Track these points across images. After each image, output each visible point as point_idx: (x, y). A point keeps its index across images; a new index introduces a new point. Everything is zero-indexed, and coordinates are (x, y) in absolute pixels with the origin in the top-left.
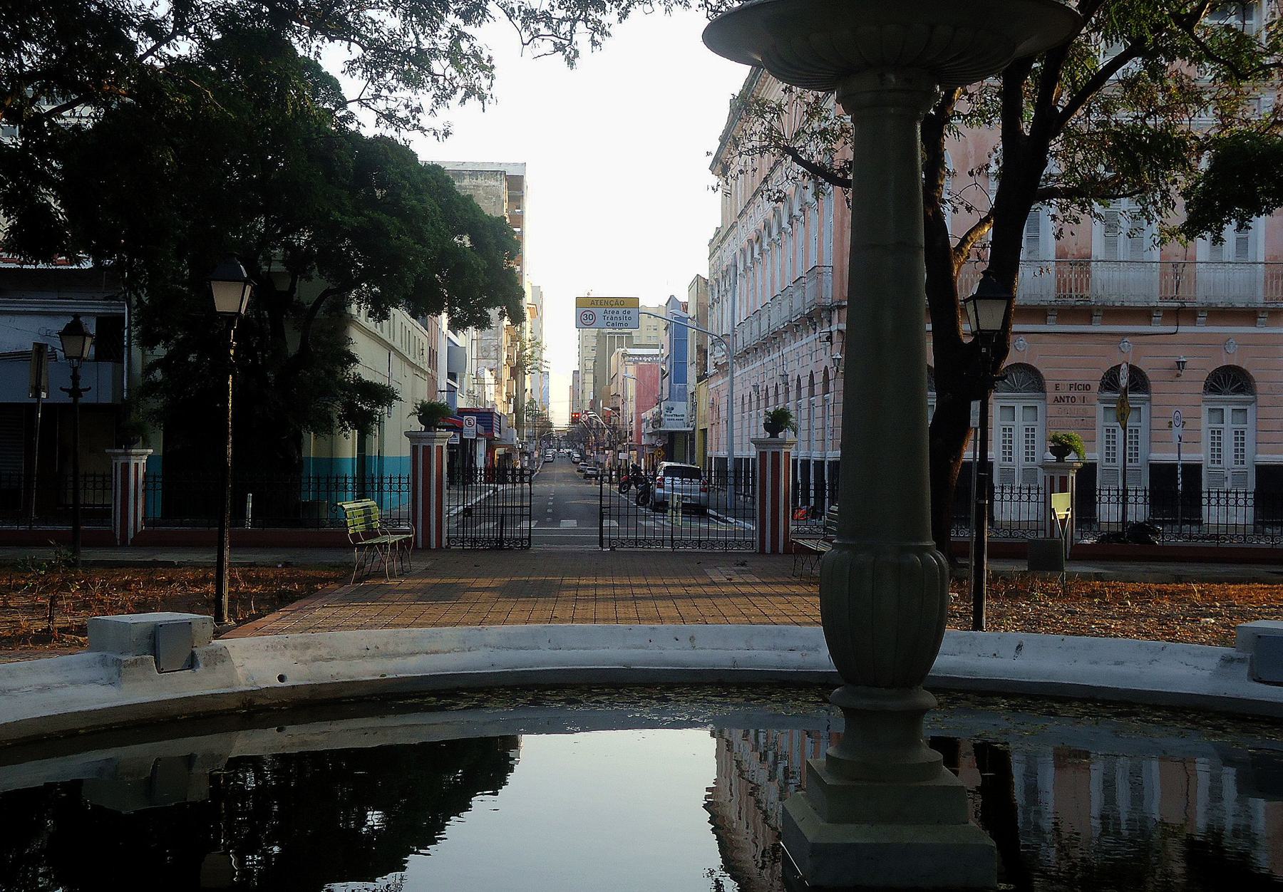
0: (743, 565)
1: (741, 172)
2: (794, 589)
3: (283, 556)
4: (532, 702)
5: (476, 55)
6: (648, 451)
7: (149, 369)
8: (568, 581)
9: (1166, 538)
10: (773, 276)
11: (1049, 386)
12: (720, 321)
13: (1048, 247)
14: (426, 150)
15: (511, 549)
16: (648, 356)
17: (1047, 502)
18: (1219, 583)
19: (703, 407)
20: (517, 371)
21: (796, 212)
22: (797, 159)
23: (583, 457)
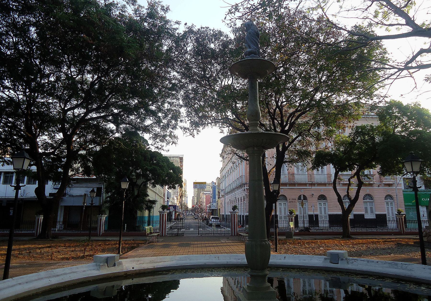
0: (228, 238)
1: (226, 158)
2: (239, 244)
3: (132, 238)
4: (185, 272)
5: (174, 136)
6: (208, 213)
7: (107, 198)
8: (192, 243)
9: (313, 230)
10: (233, 178)
11: (288, 199)
12: (223, 186)
13: (286, 172)
14: (164, 153)
15: (180, 236)
16: (208, 193)
17: (289, 224)
18: (323, 240)
19: (219, 204)
20: (181, 197)
21: (237, 165)
22: (237, 155)
23: (195, 215)
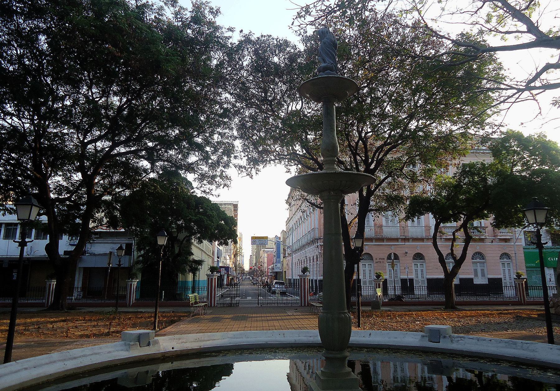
0: (296, 310)
1: (294, 205)
2: (310, 316)
3: (171, 309)
4: (240, 354)
5: (227, 176)
6: (270, 277)
7: (139, 257)
8: (249, 315)
9: (406, 299)
10: (302, 231)
11: (374, 259)
12: (289, 242)
13: (372, 223)
14: (213, 199)
15: (234, 306)
16: (270, 251)
17: (375, 291)
18: (420, 311)
19: (285, 265)
20: (235, 255)
21: (308, 214)
22: (308, 202)
23: (253, 279)
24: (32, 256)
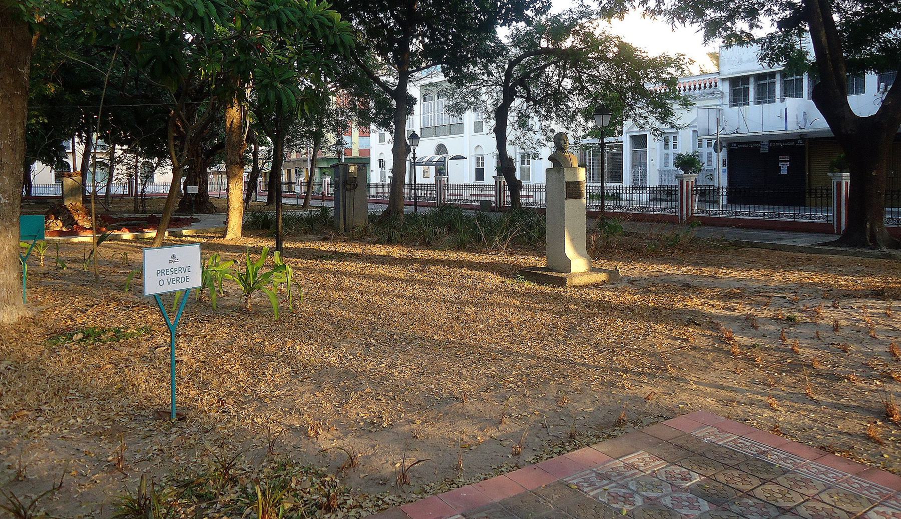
24: (806, 131)
